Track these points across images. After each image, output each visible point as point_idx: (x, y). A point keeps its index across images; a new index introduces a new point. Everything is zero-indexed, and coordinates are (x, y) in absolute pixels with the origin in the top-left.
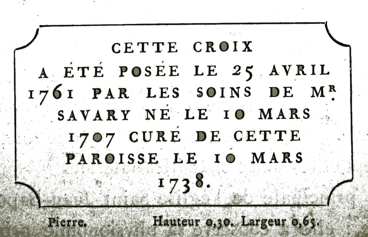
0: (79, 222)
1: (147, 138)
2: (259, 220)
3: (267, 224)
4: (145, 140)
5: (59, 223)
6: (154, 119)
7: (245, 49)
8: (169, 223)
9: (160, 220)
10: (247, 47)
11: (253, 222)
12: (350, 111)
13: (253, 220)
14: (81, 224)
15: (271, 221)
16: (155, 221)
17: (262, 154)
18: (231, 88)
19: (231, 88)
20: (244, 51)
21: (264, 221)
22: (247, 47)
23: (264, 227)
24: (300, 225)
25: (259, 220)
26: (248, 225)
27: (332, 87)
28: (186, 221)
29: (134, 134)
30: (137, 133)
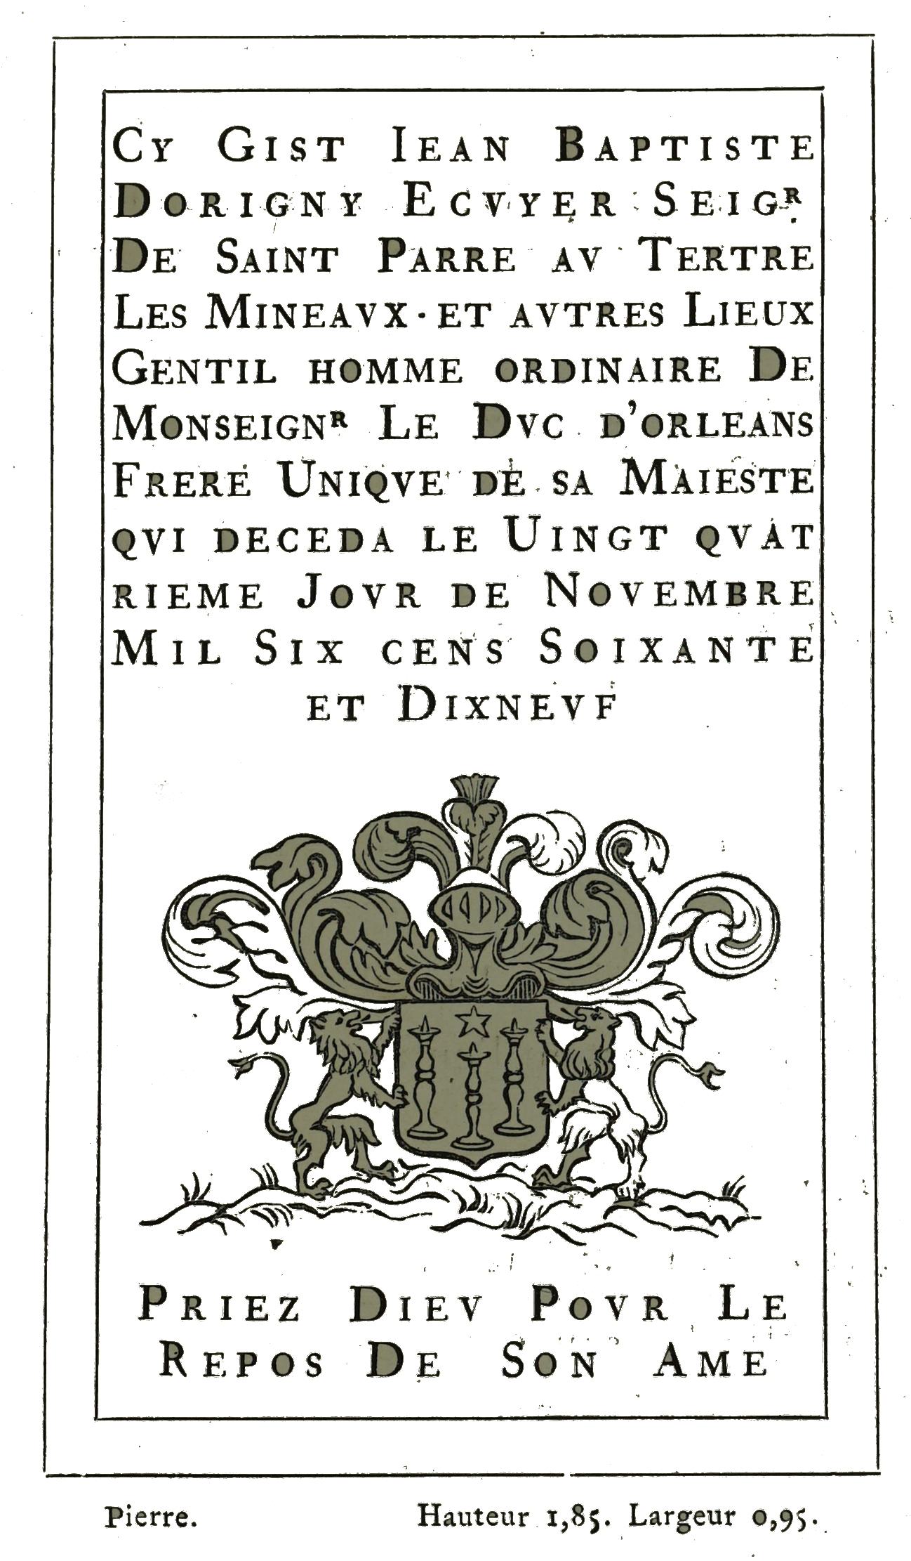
0: (178, 1517)
1: (774, 317)
2: (172, 1514)
3: (690, 1521)
4: (768, 321)
5: (133, 1521)
6: (302, 270)
7: (392, 321)
8: (456, 1519)
9: (436, 1514)
10: (396, 316)
11: (658, 1518)
12: (158, 1472)
13: (451, 1514)
14: (182, 1521)
15: (701, 1514)
16: (424, 1514)
17: (723, 1355)
18: (710, 639)
19: (710, 639)
20: (390, 325)
21: (683, 1516)
22: (396, 316)
23: (684, 1529)
24: (773, 1522)
25: (172, 1514)
26: (644, 1523)
28: (496, 1516)
29: (290, 534)
30: (296, 532)
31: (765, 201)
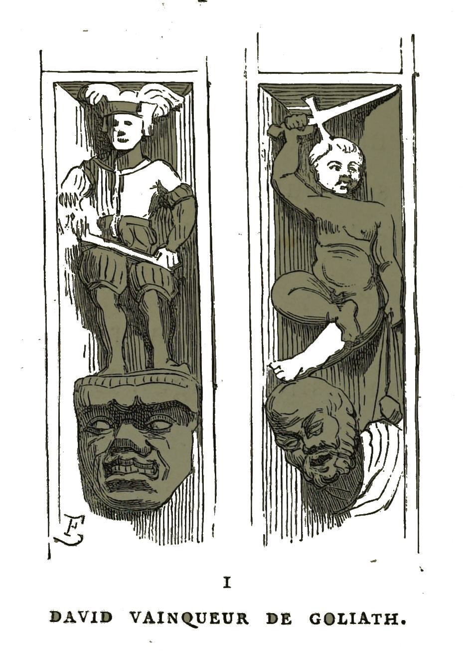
27: (242, 616)
31: (315, 618)
